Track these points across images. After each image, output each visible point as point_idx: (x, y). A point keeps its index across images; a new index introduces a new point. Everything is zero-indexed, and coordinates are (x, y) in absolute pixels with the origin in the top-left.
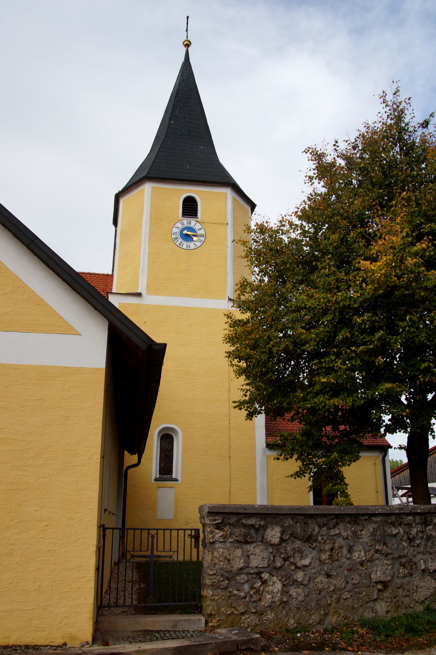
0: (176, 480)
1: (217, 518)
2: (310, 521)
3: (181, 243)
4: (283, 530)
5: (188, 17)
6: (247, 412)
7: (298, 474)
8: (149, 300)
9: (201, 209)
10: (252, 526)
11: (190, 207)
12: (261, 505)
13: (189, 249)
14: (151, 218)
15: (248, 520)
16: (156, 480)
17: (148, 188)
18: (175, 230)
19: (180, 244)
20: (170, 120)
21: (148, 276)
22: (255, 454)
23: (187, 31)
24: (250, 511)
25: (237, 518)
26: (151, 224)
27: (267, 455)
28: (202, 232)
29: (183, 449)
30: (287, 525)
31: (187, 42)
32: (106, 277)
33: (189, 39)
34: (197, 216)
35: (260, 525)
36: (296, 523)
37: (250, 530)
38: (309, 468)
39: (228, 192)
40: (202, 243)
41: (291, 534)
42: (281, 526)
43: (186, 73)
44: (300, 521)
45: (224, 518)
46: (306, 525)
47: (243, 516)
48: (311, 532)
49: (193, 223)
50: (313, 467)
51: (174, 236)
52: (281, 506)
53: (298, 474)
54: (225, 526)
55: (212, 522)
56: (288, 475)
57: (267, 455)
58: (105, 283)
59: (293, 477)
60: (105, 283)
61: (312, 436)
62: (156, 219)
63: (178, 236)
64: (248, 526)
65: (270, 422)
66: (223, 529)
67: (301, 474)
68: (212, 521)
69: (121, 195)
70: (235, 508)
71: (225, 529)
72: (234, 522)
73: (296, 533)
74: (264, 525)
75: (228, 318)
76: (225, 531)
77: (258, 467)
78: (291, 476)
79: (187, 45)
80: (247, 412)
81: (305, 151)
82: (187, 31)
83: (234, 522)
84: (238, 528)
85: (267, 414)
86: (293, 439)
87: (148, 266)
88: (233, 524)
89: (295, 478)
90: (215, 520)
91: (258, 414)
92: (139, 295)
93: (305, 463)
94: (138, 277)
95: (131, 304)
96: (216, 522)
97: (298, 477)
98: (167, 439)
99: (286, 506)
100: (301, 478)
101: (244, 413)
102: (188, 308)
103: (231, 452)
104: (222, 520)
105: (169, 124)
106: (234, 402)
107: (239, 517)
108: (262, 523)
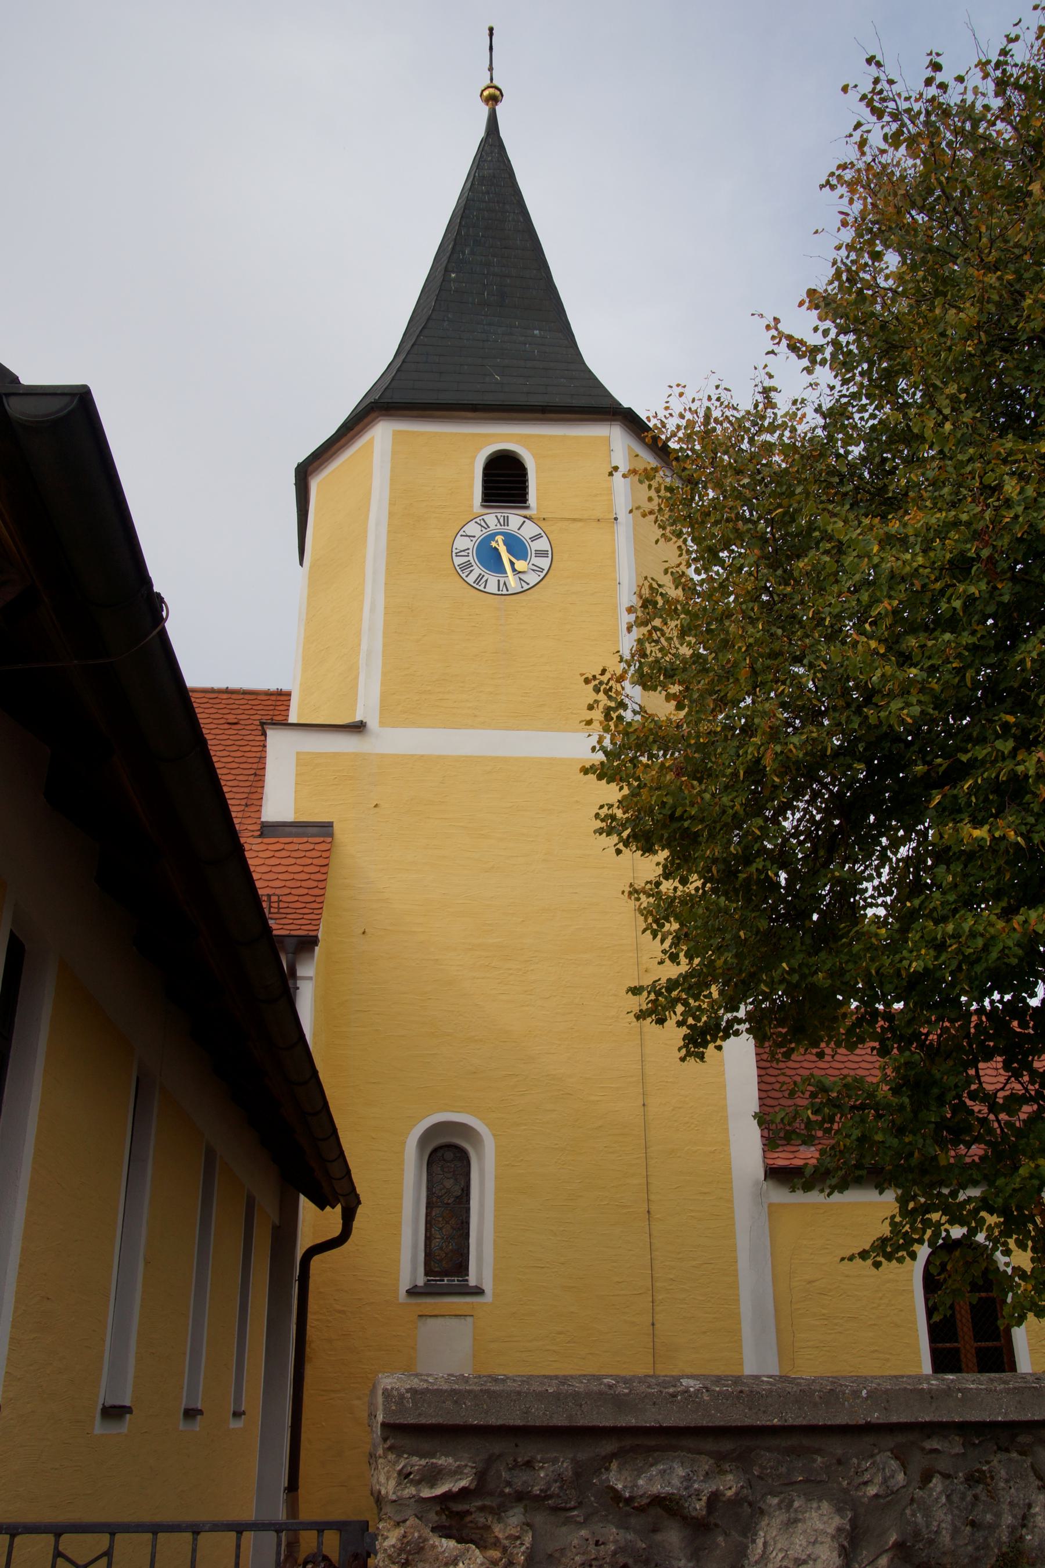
0: (479, 1292)
1: (441, 1461)
2: (999, 1465)
3: (480, 577)
4: (853, 1522)
5: (491, 30)
6: (684, 1030)
7: (889, 1249)
8: (389, 741)
9: (538, 485)
10: (666, 1506)
11: (505, 482)
12: (718, 1380)
13: (505, 592)
14: (391, 514)
15: (640, 1472)
16: (413, 1292)
17: (382, 434)
18: (461, 543)
19: (478, 580)
20: (446, 270)
21: (384, 674)
22: (731, 1201)
23: (491, 69)
24: (649, 1419)
25: (573, 1460)
26: (393, 531)
27: (770, 1205)
28: (543, 544)
29: (498, 1190)
30: (872, 1490)
31: (492, 90)
32: (273, 698)
33: (495, 82)
34: (525, 501)
35: (714, 1498)
36: (926, 1478)
37: (655, 1530)
38: (927, 1223)
39: (616, 435)
40: (542, 575)
41: (899, 1546)
42: (843, 1502)
43: (491, 161)
44: (943, 1464)
45: (490, 1461)
46: (979, 1489)
47: (609, 1447)
48: (1013, 1529)
49: (515, 519)
50: (944, 1219)
51: (458, 561)
52: (835, 1380)
53: (889, 1249)
54: (499, 1512)
55: (412, 1490)
56: (848, 1254)
57: (770, 1205)
58: (271, 713)
59: (869, 1262)
60: (271, 713)
61: (936, 1091)
62: (408, 517)
63: (472, 558)
64: (641, 1509)
65: (768, 1065)
66: (488, 1528)
67: (899, 1248)
68: (417, 1483)
69: (311, 468)
70: (557, 1396)
71: (499, 1531)
72: (555, 1488)
73: (931, 1542)
74: (737, 1501)
75: (597, 690)
76: (496, 1544)
77: (743, 1241)
78: (864, 1255)
79: (493, 98)
80: (684, 1030)
81: (828, 182)
82: (491, 69)
83: (555, 1488)
84: (581, 1525)
85: (758, 1033)
86: (862, 1107)
87: (384, 645)
88: (544, 1496)
89: (877, 1265)
90: (432, 1476)
91: (726, 1036)
92: (358, 728)
93: (911, 1205)
94: (357, 677)
95: (335, 755)
96: (439, 1491)
97: (889, 1260)
98: (447, 1159)
99: (863, 1380)
100: (901, 1260)
101: (673, 1034)
102: (505, 760)
103: (652, 1197)
104: (481, 1476)
105: (445, 279)
106: (635, 991)
107: (582, 1456)
108: (730, 1485)
